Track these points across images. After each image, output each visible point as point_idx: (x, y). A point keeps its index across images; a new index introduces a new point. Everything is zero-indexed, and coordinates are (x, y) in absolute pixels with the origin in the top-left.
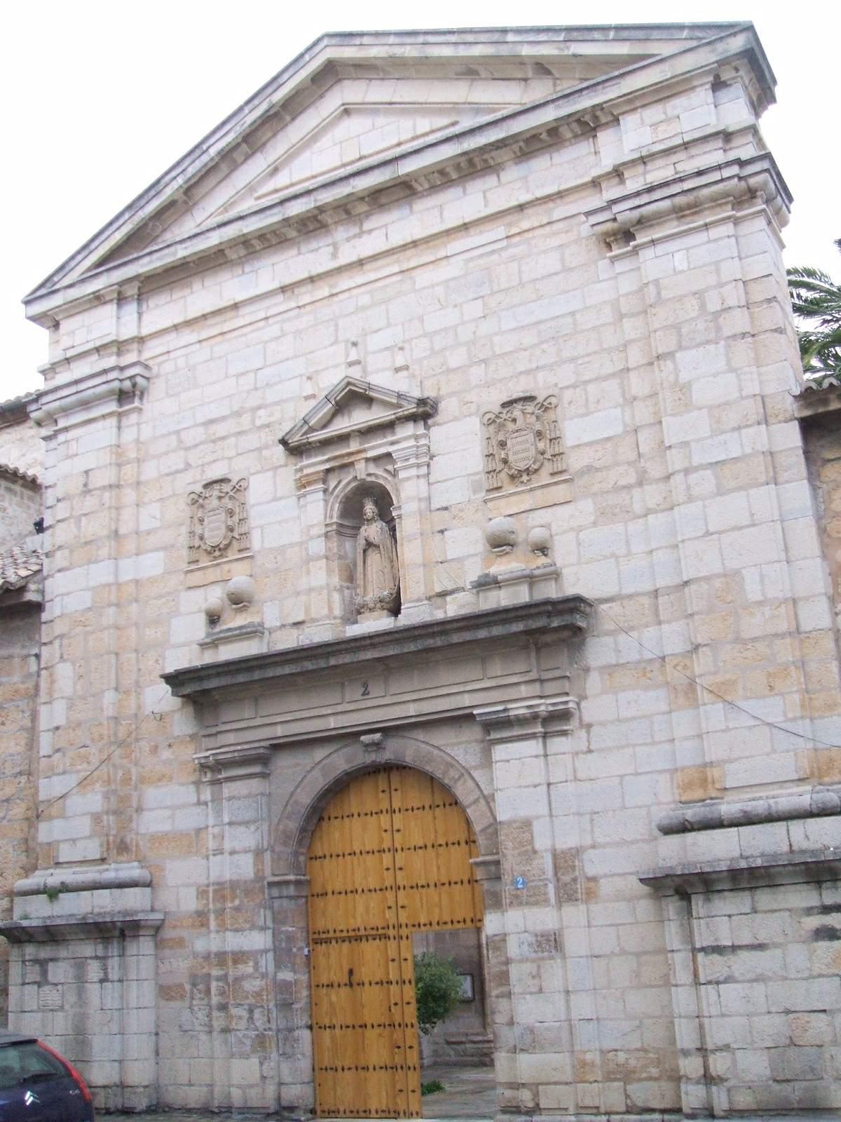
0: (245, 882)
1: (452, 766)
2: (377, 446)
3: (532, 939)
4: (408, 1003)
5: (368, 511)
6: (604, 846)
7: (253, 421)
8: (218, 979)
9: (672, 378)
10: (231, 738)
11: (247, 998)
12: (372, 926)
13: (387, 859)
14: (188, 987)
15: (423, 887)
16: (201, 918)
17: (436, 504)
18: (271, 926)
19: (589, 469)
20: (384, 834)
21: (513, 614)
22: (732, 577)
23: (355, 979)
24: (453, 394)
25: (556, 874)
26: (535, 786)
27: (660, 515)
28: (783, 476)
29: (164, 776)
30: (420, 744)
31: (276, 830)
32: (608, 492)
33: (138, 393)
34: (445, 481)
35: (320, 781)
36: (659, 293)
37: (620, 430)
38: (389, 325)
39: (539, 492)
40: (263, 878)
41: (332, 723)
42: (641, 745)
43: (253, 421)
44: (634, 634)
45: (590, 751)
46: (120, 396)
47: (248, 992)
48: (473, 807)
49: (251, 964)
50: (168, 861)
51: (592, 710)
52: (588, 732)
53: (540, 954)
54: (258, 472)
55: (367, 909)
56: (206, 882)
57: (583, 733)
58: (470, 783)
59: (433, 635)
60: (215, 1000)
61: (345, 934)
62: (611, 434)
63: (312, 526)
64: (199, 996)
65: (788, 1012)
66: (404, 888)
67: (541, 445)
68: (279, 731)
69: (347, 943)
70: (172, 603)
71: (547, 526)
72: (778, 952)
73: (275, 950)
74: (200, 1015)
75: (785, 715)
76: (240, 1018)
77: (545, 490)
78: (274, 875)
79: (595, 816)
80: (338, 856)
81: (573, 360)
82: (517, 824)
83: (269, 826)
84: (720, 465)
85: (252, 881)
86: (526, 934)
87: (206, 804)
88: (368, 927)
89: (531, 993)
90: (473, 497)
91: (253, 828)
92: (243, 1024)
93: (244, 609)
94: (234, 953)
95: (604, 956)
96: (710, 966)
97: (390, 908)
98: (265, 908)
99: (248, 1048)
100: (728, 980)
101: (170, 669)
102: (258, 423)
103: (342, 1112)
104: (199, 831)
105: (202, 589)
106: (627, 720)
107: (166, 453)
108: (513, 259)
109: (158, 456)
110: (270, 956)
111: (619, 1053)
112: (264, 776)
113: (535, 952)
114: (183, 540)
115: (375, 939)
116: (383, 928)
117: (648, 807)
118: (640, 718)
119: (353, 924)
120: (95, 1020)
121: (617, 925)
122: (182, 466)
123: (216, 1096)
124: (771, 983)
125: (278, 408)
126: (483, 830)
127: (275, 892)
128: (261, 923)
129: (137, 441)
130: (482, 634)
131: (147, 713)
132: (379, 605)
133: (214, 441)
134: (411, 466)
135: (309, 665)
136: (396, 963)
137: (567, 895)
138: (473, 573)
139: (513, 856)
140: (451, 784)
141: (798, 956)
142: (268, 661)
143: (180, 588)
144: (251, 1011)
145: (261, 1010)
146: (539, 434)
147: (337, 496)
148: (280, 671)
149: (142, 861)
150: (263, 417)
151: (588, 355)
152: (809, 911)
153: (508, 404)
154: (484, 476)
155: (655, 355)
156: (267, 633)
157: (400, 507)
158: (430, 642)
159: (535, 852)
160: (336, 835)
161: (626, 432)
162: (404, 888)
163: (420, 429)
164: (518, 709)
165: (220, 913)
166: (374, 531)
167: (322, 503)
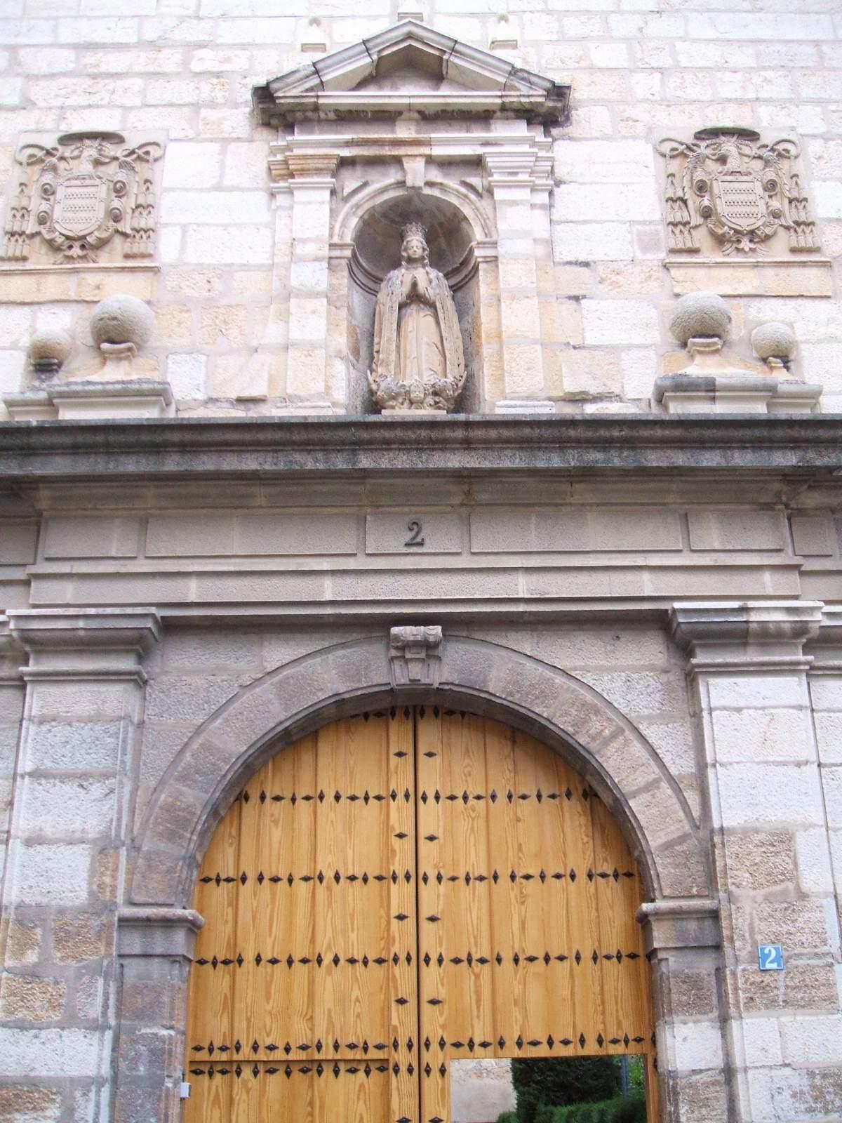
0: (62, 911)
2: (455, 142)
3: (800, 1082)
10: (68, 592)
12: (352, 1039)
13: (400, 896)
15: (482, 961)
17: (565, 252)
20: (396, 843)
21: (779, 433)
26: (799, 765)
30: (522, 660)
31: (150, 804)
34: (585, 222)
35: (273, 712)
39: (770, 272)
40: (110, 907)
41: (329, 589)
48: (645, 797)
55: (342, 1000)
58: (637, 748)
59: (605, 444)
61: (279, 1055)
63: (304, 241)
66: (440, 961)
67: (775, 204)
68: (193, 591)
69: (279, 1076)
73: (115, 1080)
77: (783, 272)
80: (275, 880)
82: (762, 837)
83: (134, 792)
86: (787, 1071)
88: (342, 1043)
90: (639, 256)
91: (97, 790)
93: (129, 355)
97: (401, 1001)
98: (107, 977)
102: (196, 67)
105: (26, 308)
112: (139, 681)
113: (810, 1110)
115: (353, 1071)
116: (380, 1047)
119: (300, 1033)
126: (668, 846)
127: (134, 942)
128: (95, 1011)
130: (711, 459)
132: (430, 400)
133: (94, 77)
134: (521, 185)
135: (309, 462)
139: (754, 900)
140: (593, 746)
142: (205, 437)
146: (771, 187)
147: (358, 206)
148: (231, 463)
150: (206, 60)
154: (663, 231)
158: (595, 457)
159: (803, 896)
160: (272, 835)
162: (440, 961)
163: (538, 134)
164: (771, 615)
167: (326, 210)
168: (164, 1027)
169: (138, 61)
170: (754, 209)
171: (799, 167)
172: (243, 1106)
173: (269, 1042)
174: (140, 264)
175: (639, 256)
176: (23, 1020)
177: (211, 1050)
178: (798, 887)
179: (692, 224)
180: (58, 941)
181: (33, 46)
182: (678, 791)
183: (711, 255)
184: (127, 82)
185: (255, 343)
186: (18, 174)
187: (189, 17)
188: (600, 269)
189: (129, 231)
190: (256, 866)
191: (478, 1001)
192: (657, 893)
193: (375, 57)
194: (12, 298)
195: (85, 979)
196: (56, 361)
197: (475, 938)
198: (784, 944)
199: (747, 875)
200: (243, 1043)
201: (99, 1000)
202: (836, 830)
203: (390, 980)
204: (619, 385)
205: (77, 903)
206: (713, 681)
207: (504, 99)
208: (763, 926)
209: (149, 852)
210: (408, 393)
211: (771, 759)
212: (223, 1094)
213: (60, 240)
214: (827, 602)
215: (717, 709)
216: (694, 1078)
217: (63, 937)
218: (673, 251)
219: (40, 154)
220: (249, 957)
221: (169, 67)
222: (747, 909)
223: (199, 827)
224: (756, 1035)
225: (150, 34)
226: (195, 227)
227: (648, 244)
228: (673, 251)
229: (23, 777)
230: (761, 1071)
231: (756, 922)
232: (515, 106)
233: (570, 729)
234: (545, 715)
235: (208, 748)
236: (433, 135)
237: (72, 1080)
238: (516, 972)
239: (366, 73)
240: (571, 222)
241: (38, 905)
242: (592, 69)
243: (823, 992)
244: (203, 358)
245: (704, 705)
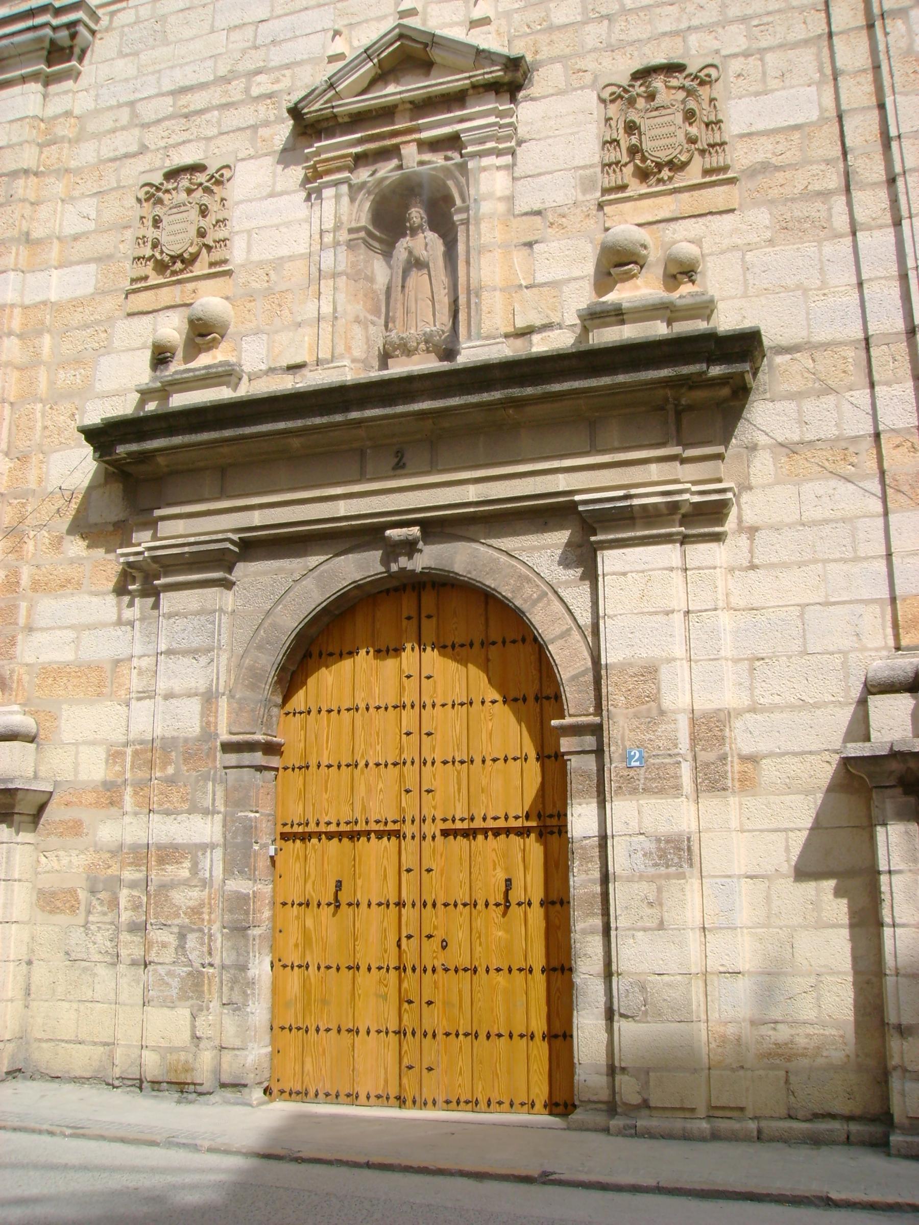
0: (186, 740)
1: (529, 580)
2: (438, 126)
3: (650, 846)
6: (772, 709)
7: (247, 90)
8: (133, 885)
11: (178, 916)
12: (378, 817)
14: (82, 895)
16: (110, 795)
17: (522, 206)
18: (222, 809)
19: (765, 168)
23: (344, 898)
24: (553, 60)
25: (693, 748)
27: (876, 233)
29: (69, 581)
32: (793, 200)
33: (77, 51)
34: (540, 174)
37: (814, 116)
39: (685, 196)
42: (835, 561)
43: (247, 90)
45: (753, 567)
46: (49, 53)
47: (180, 908)
48: (560, 642)
49: (187, 864)
50: (65, 706)
51: (748, 508)
52: (752, 539)
53: (663, 870)
54: (251, 157)
56: (123, 739)
57: (743, 541)
58: (557, 606)
62: (800, 121)
64: (99, 908)
67: (693, 131)
69: (336, 840)
70: (104, 335)
71: (697, 242)
73: (225, 845)
74: (99, 937)
76: (164, 945)
78: (231, 733)
79: (757, 663)
81: (744, 19)
87: (131, 624)
89: (645, 930)
92: (168, 956)
94: (160, 847)
95: (763, 877)
97: (408, 791)
99: (174, 992)
101: (94, 417)
102: (255, 91)
103: (363, 1097)
104: (117, 662)
105: (151, 316)
106: (814, 523)
107: (114, 131)
109: (97, 136)
110: (218, 853)
111: (779, 1026)
114: (128, 249)
117: (845, 653)
118: (836, 521)
121: (785, 830)
122: (134, 148)
123: (117, 1062)
125: (287, 73)
126: (574, 678)
127: (232, 758)
131: (50, 489)
133: (186, 116)
137: (711, 781)
143: (117, 313)
144: (182, 937)
145: (197, 934)
146: (689, 116)
149: (27, 707)
150: (262, 85)
151: (769, 14)
153: (644, 74)
156: (245, 379)
157: (467, 209)
159: (662, 713)
165: (141, 786)
166: (427, 243)
168: (252, 811)
169: (214, 96)
171: (717, 90)
172: (313, 861)
173: (326, 820)
174: (221, 271)
175: (581, 198)
176: (168, 809)
177: (292, 826)
178: (659, 705)
179: (623, 162)
180: (185, 760)
181: (145, 98)
183: (636, 188)
184: (208, 116)
185: (299, 319)
186: (138, 211)
187: (250, 48)
189: (212, 244)
190: (317, 702)
191: (459, 790)
192: (566, 712)
193: (375, 61)
194: (140, 309)
195: (201, 783)
196: (169, 354)
197: (458, 746)
198: (646, 748)
199: (623, 698)
200: (311, 821)
202: (697, 661)
204: (560, 315)
205: (195, 734)
206: (606, 553)
207: (474, 80)
208: (632, 735)
209: (240, 699)
210: (405, 345)
211: (646, 610)
212: (301, 854)
213: (167, 259)
214: (694, 483)
215: (608, 574)
216: (585, 842)
218: (605, 191)
219: (153, 190)
220: (313, 763)
221: (237, 97)
222: (621, 723)
223: (270, 680)
225: (222, 71)
226: (257, 231)
227: (587, 185)
228: (605, 191)
229: (161, 654)
230: (623, 838)
231: (627, 732)
232: (482, 82)
233: (509, 595)
234: (493, 586)
235: (274, 625)
236: (420, 122)
237: (195, 845)
238: (484, 769)
239: (373, 74)
240: (529, 176)
241: (173, 738)
242: (552, 29)
243: (672, 782)
244: (265, 337)
245: (600, 572)
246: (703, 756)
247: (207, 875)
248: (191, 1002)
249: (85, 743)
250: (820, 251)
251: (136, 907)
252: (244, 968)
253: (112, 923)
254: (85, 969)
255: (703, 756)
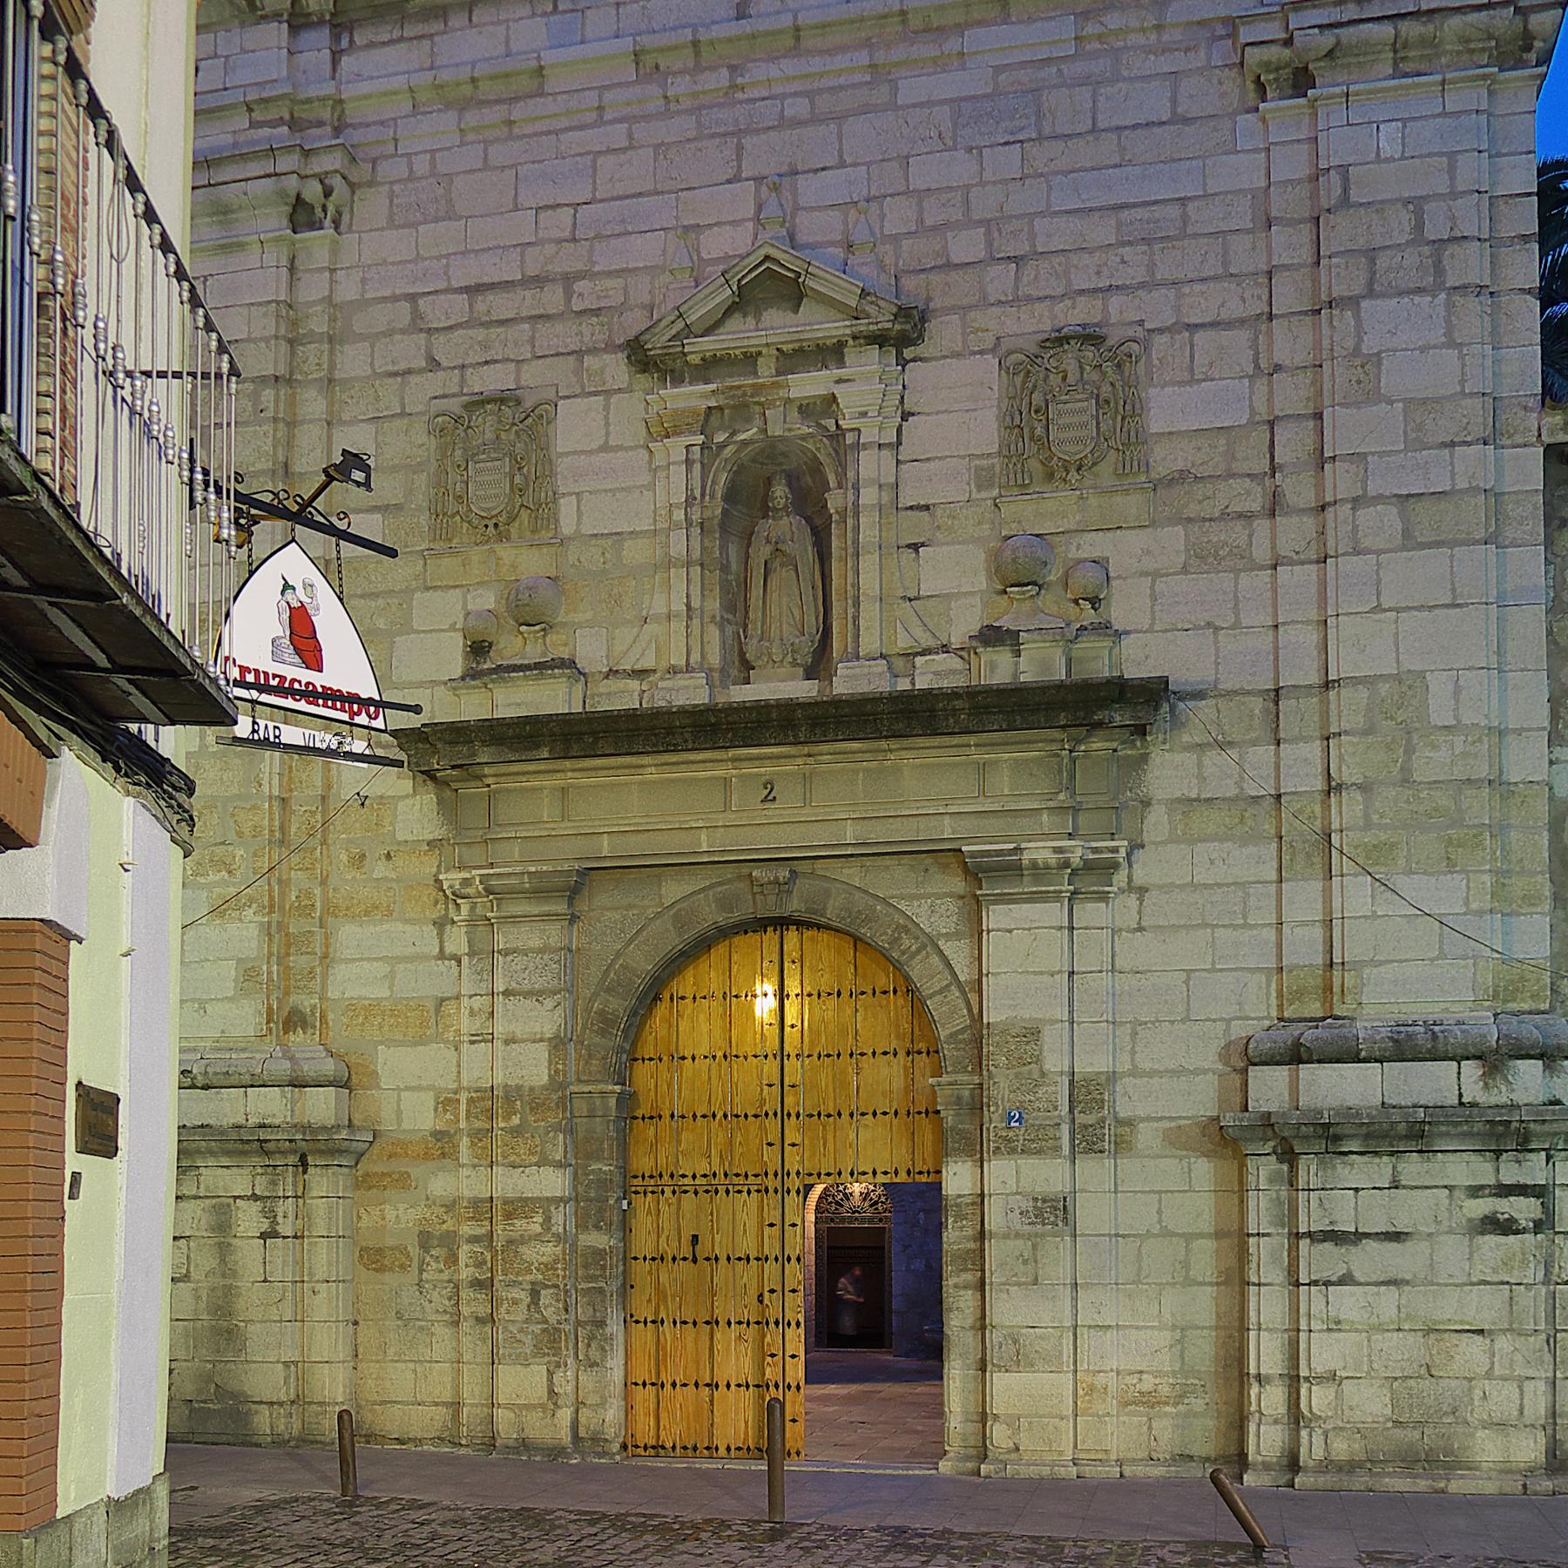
0: (532, 1089)
4: (794, 1291)
5: (778, 494)
6: (1152, 1074)
8: (474, 1239)
9: (1350, 343)
14: (414, 1251)
16: (441, 1145)
22: (1411, 684)
25: (1071, 1111)
28: (1510, 533)
31: (588, 1010)
36: (1346, 190)
38: (842, 164)
44: (1234, 753)
45: (1140, 929)
48: (938, 998)
49: (539, 1219)
57: (1132, 900)
58: (935, 959)
60: (466, 1273)
65: (1428, 1332)
72: (1424, 1246)
75: (1467, 902)
76: (515, 1302)
84: (1412, 500)
85: (543, 1087)
89: (1019, 1284)
91: (549, 1003)
92: (520, 1314)
96: (1318, 1260)
97: (770, 1144)
100: (1346, 1280)
102: (577, 305)
103: (722, 1451)
108: (1084, 81)
109: (373, 338)
111: (1145, 1376)
120: (251, 1299)
121: (1159, 1192)
124: (1407, 1288)
129: (329, 300)
136: (776, 1230)
137: (1087, 1142)
138: (964, 624)
141: (1452, 1253)
144: (535, 1294)
152: (1475, 1191)
155: (1324, 297)
159: (1043, 1074)
161: (1252, 423)
169: (526, 303)
170: (1084, 433)
180: (532, 1109)
182: (964, 993)
188: (939, 512)
201: (561, 1149)
203: (763, 1129)
217: (535, 1106)
224: (1001, 1172)
246: (1081, 1119)
247: (561, 1230)
248: (547, 1359)
249: (407, 1088)
250: (1236, 584)
251: (480, 1265)
252: (602, 1324)
253: (450, 1281)
254: (422, 1328)
255: (1081, 1119)
